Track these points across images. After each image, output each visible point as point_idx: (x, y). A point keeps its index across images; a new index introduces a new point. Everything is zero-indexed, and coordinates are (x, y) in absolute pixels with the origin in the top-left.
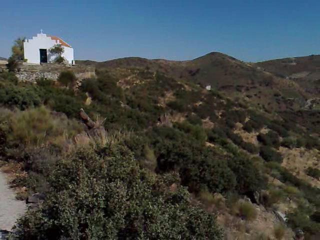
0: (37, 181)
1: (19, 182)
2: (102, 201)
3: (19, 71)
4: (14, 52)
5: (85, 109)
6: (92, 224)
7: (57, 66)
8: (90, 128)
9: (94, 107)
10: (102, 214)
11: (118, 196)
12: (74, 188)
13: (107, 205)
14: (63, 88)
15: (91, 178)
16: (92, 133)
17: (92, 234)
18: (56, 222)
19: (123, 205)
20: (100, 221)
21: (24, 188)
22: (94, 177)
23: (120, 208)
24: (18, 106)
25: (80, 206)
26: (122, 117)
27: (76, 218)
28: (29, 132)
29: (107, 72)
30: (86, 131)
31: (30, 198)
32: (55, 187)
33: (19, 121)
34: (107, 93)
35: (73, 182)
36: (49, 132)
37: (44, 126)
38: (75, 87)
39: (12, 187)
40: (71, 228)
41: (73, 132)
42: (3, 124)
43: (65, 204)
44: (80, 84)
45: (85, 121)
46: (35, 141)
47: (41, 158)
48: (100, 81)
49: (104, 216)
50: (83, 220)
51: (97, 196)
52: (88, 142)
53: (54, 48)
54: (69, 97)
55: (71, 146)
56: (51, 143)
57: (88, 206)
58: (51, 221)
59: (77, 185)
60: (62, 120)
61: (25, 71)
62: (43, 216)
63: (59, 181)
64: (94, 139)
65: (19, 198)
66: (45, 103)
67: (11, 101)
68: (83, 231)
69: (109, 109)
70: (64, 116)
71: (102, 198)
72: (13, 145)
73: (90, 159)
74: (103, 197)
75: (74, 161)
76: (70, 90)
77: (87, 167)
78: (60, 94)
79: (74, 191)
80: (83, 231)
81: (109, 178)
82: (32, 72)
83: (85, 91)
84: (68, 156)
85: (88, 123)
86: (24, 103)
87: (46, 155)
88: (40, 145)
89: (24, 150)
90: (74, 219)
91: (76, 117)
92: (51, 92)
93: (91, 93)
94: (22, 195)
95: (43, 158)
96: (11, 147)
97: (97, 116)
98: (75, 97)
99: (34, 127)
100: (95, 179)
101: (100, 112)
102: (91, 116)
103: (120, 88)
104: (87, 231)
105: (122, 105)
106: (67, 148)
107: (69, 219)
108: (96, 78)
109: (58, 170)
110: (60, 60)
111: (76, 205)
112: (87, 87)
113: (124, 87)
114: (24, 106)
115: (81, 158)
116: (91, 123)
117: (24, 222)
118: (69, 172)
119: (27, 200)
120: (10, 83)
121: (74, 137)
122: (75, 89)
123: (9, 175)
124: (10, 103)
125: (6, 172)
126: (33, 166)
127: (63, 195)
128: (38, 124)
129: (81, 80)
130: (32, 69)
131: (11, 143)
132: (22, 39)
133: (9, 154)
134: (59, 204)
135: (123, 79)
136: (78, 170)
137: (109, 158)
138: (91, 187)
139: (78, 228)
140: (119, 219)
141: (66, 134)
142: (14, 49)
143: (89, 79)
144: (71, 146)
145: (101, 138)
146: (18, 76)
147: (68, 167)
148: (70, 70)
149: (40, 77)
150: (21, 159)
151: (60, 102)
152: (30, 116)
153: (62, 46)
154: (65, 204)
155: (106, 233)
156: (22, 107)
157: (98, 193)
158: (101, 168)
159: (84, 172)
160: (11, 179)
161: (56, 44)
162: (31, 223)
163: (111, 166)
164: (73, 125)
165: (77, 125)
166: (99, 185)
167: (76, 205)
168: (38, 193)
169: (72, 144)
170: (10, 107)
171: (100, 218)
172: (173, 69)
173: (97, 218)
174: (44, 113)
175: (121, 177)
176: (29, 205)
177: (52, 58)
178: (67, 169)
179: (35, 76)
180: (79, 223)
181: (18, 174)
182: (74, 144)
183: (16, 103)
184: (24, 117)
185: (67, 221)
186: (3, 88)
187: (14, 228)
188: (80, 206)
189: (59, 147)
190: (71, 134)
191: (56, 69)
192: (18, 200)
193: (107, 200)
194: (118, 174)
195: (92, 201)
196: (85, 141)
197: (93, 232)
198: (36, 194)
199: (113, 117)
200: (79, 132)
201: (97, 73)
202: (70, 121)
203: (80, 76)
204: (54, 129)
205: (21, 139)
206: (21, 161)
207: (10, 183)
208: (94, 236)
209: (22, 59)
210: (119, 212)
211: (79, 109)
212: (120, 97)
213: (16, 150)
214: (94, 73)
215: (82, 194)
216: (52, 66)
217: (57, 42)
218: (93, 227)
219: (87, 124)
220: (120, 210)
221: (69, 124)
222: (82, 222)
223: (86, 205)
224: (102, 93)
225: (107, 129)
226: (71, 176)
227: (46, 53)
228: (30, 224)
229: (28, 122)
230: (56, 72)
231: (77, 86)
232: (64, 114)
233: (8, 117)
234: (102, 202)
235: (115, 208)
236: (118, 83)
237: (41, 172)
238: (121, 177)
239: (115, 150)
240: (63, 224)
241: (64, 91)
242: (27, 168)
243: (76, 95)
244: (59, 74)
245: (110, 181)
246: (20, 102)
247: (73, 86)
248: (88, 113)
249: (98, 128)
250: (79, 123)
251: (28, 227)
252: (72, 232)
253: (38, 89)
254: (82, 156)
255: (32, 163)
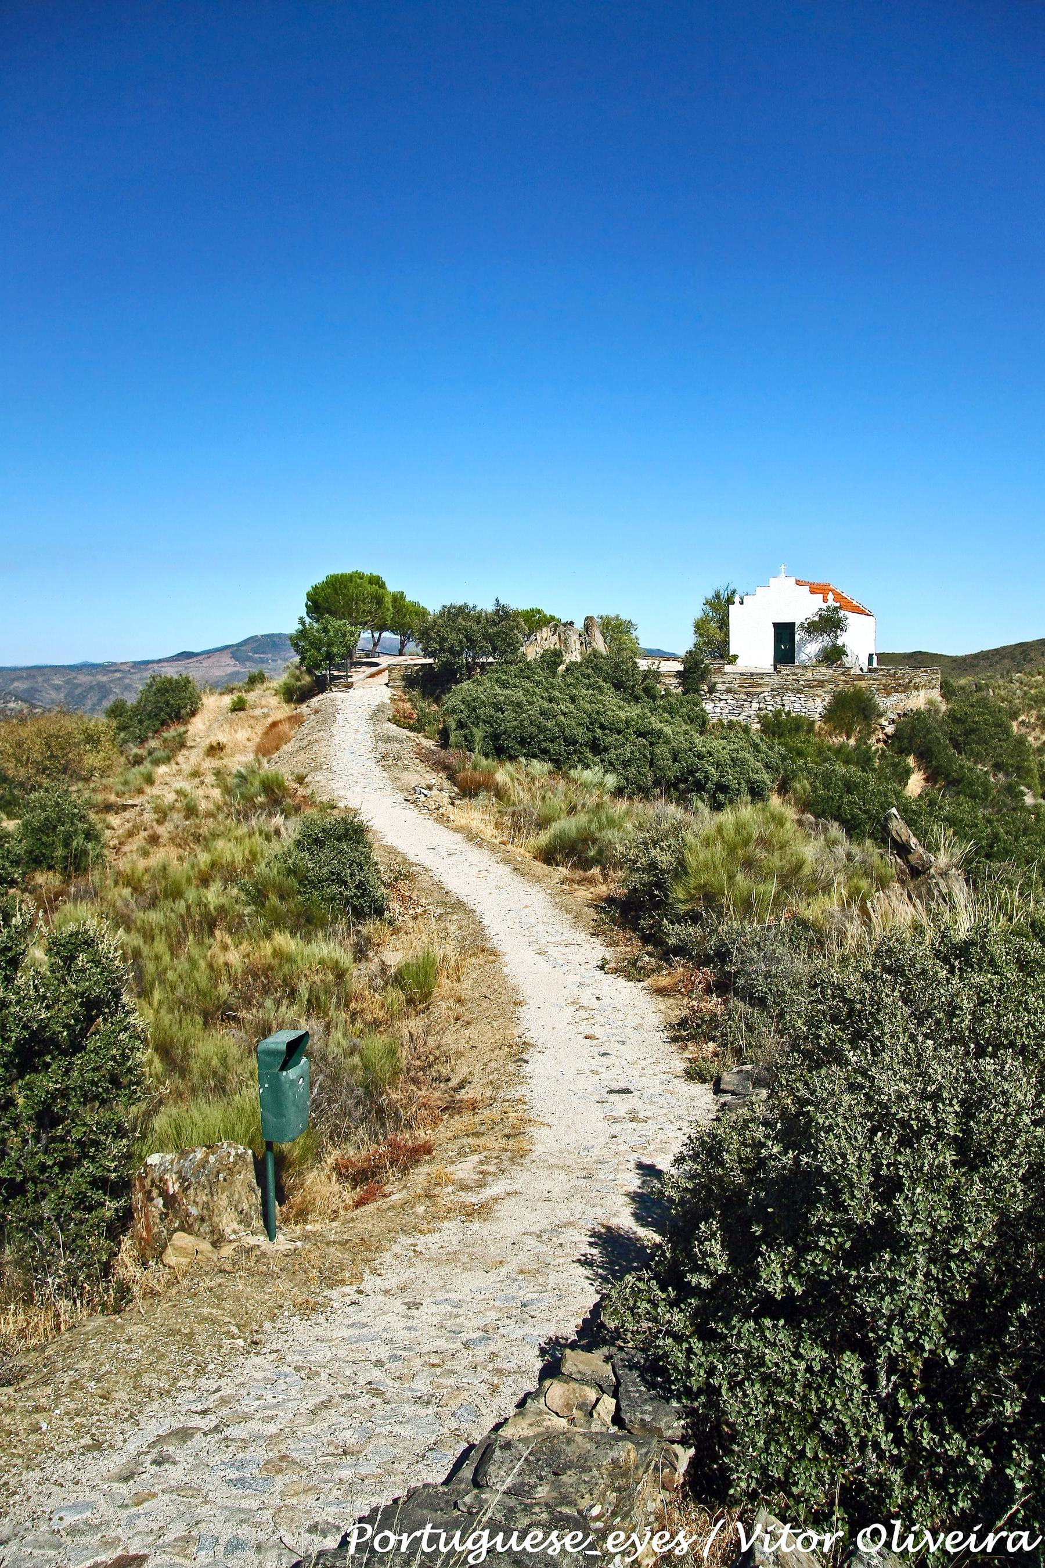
0: (750, 1028)
1: (699, 1026)
2: (950, 1113)
3: (712, 690)
4: (701, 635)
5: (904, 809)
6: (914, 1182)
7: (825, 672)
8: (917, 872)
9: (932, 803)
10: (949, 1156)
11: (1006, 1105)
12: (864, 1064)
13: (967, 1131)
14: (837, 740)
15: (920, 1039)
16: (923, 890)
17: (914, 1214)
18: (804, 1159)
19: (1018, 1136)
20: (940, 1177)
21: (711, 1046)
22: (926, 1036)
23: (1012, 1145)
24: (706, 796)
25: (880, 1120)
26: (1023, 840)
27: (867, 1156)
28: (731, 877)
29: (979, 688)
30: (903, 882)
31: (726, 1077)
32: (807, 1055)
33: (707, 842)
34: (979, 758)
35: (862, 1044)
36: (791, 878)
37: (776, 861)
38: (872, 740)
39: (675, 1039)
40: (851, 1185)
41: (864, 884)
42: (662, 849)
43: (835, 1110)
44: (890, 730)
45: (903, 849)
46: (747, 906)
47: (764, 957)
48: (953, 717)
49: (955, 1164)
50: (888, 1165)
51: (936, 1097)
52: (909, 918)
53: (817, 619)
54: (854, 771)
55: (854, 928)
56: (794, 915)
57: (904, 1124)
58: (790, 1154)
59: (875, 1054)
60: (831, 843)
61: (729, 691)
62: (767, 1137)
63: (819, 1037)
64: (929, 910)
65: (695, 1074)
66: (783, 789)
67: (686, 781)
68: (886, 1199)
69: (981, 812)
70: (836, 830)
71: (951, 1105)
72: (686, 914)
73: (917, 976)
74: (954, 1102)
75: (866, 976)
76: (857, 747)
77: (906, 1001)
78: (826, 759)
79: (864, 1073)
80: (886, 1199)
81: (977, 1044)
82: (747, 694)
83: (903, 752)
84: (844, 960)
85: (913, 859)
86: (722, 788)
87: (780, 950)
88: (761, 921)
89: (716, 930)
90: (860, 1159)
91: (872, 836)
92: (800, 754)
93: (925, 757)
94: (703, 1065)
95: (772, 959)
96: (678, 920)
97: (942, 834)
98: (874, 770)
99: (749, 864)
100: (930, 1042)
101: (951, 821)
102: (922, 834)
103: (1021, 741)
104: (899, 1201)
105: (1029, 800)
106: (842, 933)
107: (844, 1156)
108: (943, 707)
109: (818, 1001)
110: (833, 655)
111: (868, 1116)
112: (913, 737)
113: (1036, 739)
114: (721, 797)
115: (888, 970)
116: (921, 858)
117: (707, 1149)
118: (851, 1013)
119: (718, 1082)
120: (684, 727)
121: (864, 901)
122: (875, 743)
123: (672, 1001)
124: (682, 786)
125: (661, 992)
126: (741, 982)
127: (829, 1081)
128: (760, 853)
129: (895, 717)
130: (751, 681)
131: (682, 908)
132: (724, 596)
133: (672, 941)
134: (816, 1106)
135: (1034, 712)
136: (879, 1006)
137: (977, 979)
138: (918, 1067)
139: (873, 1186)
140: (1005, 1180)
141: (840, 890)
142: (700, 627)
143: (918, 713)
144: (854, 928)
145: (953, 908)
146: (708, 707)
147: (849, 995)
148: (863, 684)
149: (770, 708)
150: (707, 955)
151: (826, 787)
152: (739, 827)
153: (842, 613)
154: (835, 1110)
155: (959, 1217)
156: (713, 797)
157: (941, 1087)
158: (952, 1010)
159: (895, 1021)
160: (676, 1015)
161: (824, 606)
162: (728, 1151)
163: (982, 1003)
164: (864, 862)
165: (876, 860)
166: (941, 1061)
167: (868, 1116)
168: (749, 1067)
169: (857, 922)
170: (682, 800)
171: (942, 1167)
172: (75, 699)
173: (931, 1165)
174: (779, 821)
175: (1019, 1043)
176: (722, 1100)
177: (809, 649)
178: (845, 1001)
179: (755, 706)
180: (875, 1172)
181: (695, 1003)
182: (864, 923)
183: (700, 787)
184: (720, 829)
185: (840, 1162)
186: (667, 742)
187: (679, 1160)
188: (880, 1120)
189: (818, 930)
190: (858, 890)
191: (821, 684)
192: (692, 1078)
193: (968, 1111)
194: (1007, 1033)
195: (918, 1110)
196: (898, 911)
197: (920, 1206)
198: (744, 1067)
199: (996, 837)
200: (882, 883)
201: (947, 691)
202: (855, 849)
203: (893, 706)
204: (806, 870)
205: (710, 897)
206: (706, 964)
207: (672, 1026)
208: (920, 1221)
209: (722, 657)
210: (1005, 1158)
211: (885, 807)
212: (1022, 771)
213: (694, 931)
214: (936, 694)
215: (891, 1084)
216: (809, 675)
217: (825, 600)
218: (918, 1190)
219: (907, 862)
220: (1010, 1152)
221: (849, 856)
222: (884, 1172)
223: (898, 1121)
224: (963, 760)
225: (972, 879)
226: (857, 1022)
227: (793, 634)
228: (726, 1156)
229: (731, 849)
230: (819, 691)
231: (881, 736)
232: (836, 824)
233: (676, 830)
234: (951, 1119)
235: (993, 1143)
236: (1014, 724)
237: (762, 1002)
238: (1019, 1043)
239: (998, 950)
240: (825, 1169)
241: (839, 751)
242: (723, 986)
243: (877, 763)
244: (828, 698)
245: (981, 1053)
246: (710, 785)
247: (870, 733)
248: (910, 823)
249: (944, 874)
250: (882, 856)
251: (721, 1164)
252: (853, 1197)
253: (763, 747)
254: (891, 963)
255: (738, 972)
